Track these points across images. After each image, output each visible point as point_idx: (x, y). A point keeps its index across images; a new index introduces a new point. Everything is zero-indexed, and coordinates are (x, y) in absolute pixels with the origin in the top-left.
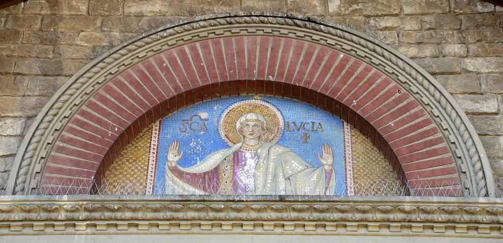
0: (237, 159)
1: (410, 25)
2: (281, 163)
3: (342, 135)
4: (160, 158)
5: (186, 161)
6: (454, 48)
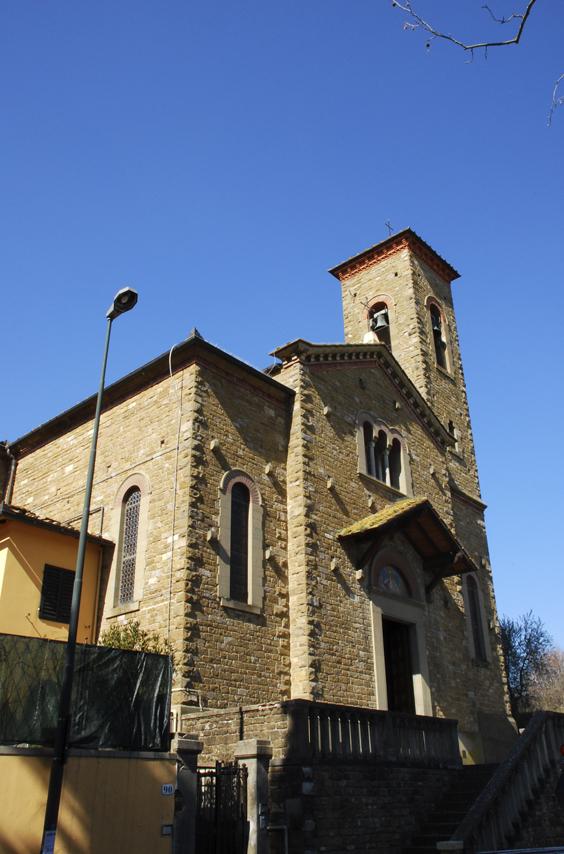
3: (400, 580)
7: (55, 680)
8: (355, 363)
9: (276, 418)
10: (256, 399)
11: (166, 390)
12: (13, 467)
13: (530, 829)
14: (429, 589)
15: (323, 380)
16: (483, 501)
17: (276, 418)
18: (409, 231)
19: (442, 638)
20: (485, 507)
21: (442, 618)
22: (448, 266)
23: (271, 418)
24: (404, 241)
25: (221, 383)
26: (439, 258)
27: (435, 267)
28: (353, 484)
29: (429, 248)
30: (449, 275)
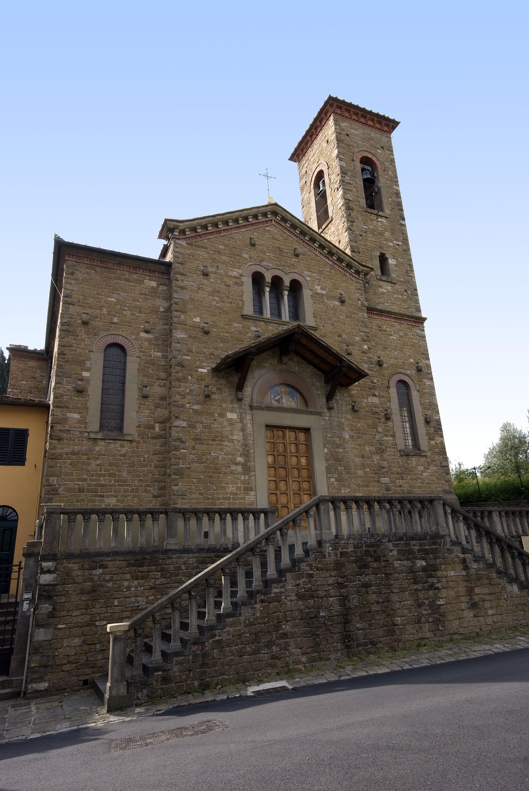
0: (282, 397)
1: (308, 375)
2: (288, 399)
4: (271, 396)
5: (274, 397)
6: (314, 380)
7: (436, 468)
8: (245, 226)
9: (158, 287)
10: (135, 276)
11: (316, 296)
12: (353, 365)
13: (258, 606)
14: (330, 397)
15: (202, 247)
16: (424, 315)
17: (158, 287)
18: (330, 98)
19: (347, 437)
20: (425, 319)
21: (349, 420)
22: (387, 119)
23: (153, 288)
24: (331, 110)
25: (95, 271)
26: (370, 113)
27: (370, 123)
28: (236, 325)
29: (357, 107)
30: (388, 126)
